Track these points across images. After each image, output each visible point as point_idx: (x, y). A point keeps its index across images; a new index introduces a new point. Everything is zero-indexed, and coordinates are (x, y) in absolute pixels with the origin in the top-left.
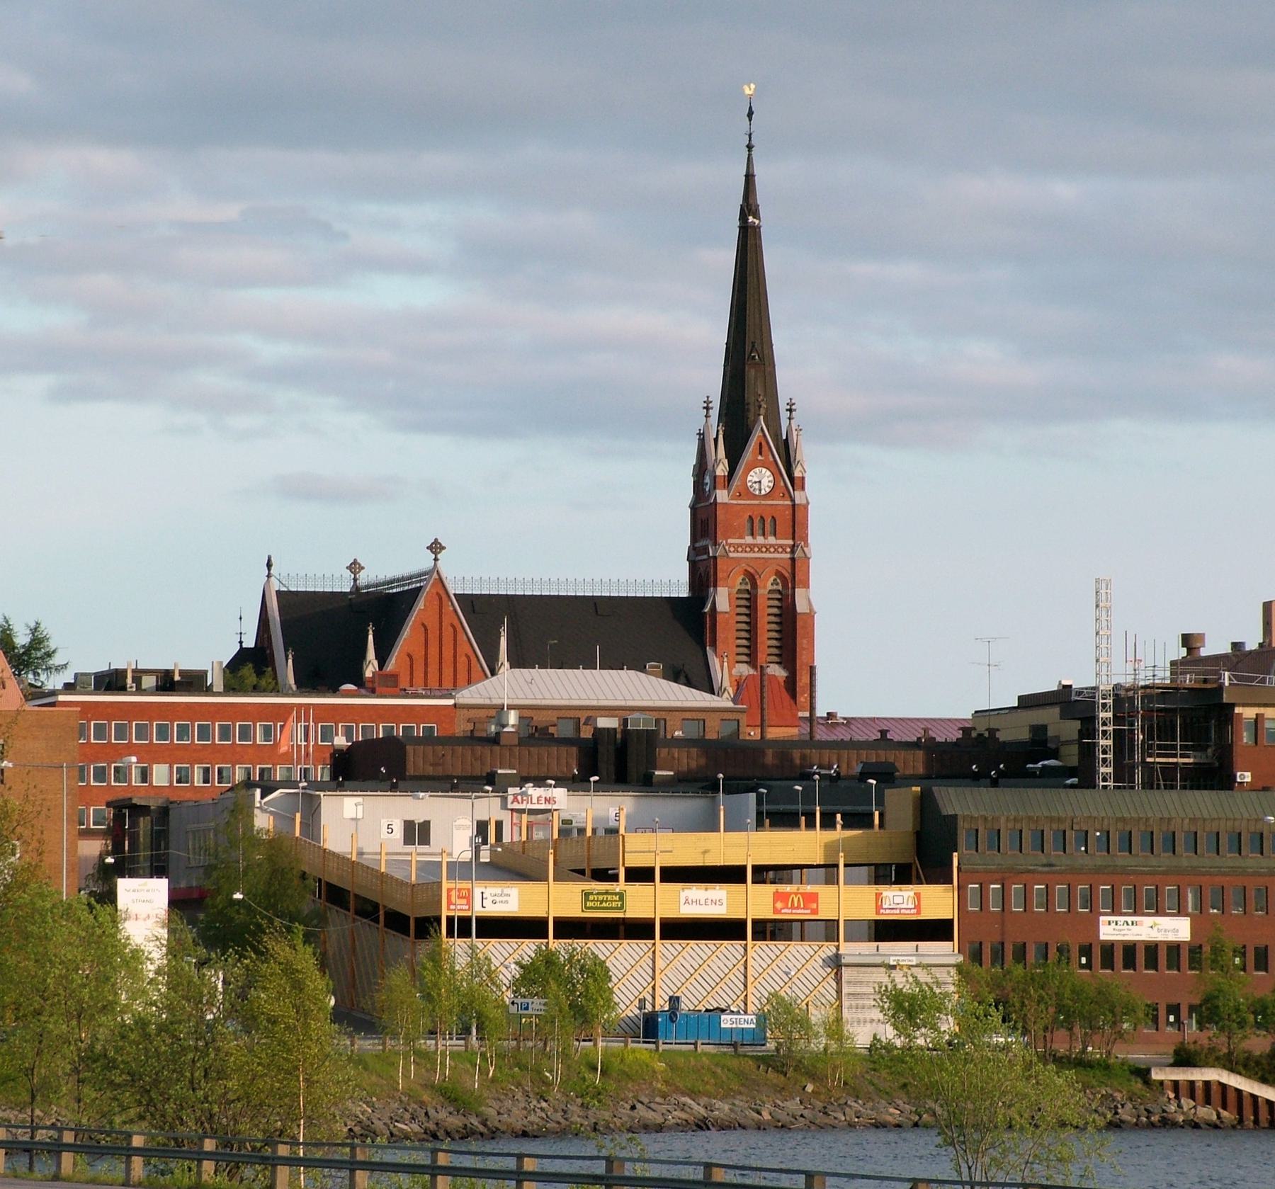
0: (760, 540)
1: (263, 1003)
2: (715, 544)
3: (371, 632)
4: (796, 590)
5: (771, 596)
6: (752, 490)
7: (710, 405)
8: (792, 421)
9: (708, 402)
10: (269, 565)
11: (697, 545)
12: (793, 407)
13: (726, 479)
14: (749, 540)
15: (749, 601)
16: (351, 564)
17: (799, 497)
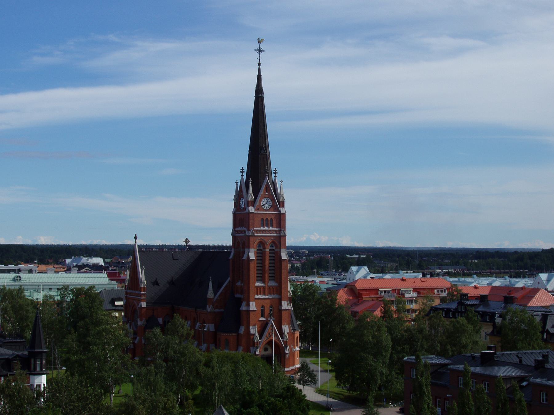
0: (266, 228)
1: (283, 370)
2: (249, 230)
3: (211, 279)
4: (282, 249)
5: (270, 252)
7: (243, 171)
9: (242, 169)
10: (136, 238)
11: (237, 229)
12: (276, 172)
13: (253, 202)
14: (262, 228)
15: (260, 254)
17: (282, 210)
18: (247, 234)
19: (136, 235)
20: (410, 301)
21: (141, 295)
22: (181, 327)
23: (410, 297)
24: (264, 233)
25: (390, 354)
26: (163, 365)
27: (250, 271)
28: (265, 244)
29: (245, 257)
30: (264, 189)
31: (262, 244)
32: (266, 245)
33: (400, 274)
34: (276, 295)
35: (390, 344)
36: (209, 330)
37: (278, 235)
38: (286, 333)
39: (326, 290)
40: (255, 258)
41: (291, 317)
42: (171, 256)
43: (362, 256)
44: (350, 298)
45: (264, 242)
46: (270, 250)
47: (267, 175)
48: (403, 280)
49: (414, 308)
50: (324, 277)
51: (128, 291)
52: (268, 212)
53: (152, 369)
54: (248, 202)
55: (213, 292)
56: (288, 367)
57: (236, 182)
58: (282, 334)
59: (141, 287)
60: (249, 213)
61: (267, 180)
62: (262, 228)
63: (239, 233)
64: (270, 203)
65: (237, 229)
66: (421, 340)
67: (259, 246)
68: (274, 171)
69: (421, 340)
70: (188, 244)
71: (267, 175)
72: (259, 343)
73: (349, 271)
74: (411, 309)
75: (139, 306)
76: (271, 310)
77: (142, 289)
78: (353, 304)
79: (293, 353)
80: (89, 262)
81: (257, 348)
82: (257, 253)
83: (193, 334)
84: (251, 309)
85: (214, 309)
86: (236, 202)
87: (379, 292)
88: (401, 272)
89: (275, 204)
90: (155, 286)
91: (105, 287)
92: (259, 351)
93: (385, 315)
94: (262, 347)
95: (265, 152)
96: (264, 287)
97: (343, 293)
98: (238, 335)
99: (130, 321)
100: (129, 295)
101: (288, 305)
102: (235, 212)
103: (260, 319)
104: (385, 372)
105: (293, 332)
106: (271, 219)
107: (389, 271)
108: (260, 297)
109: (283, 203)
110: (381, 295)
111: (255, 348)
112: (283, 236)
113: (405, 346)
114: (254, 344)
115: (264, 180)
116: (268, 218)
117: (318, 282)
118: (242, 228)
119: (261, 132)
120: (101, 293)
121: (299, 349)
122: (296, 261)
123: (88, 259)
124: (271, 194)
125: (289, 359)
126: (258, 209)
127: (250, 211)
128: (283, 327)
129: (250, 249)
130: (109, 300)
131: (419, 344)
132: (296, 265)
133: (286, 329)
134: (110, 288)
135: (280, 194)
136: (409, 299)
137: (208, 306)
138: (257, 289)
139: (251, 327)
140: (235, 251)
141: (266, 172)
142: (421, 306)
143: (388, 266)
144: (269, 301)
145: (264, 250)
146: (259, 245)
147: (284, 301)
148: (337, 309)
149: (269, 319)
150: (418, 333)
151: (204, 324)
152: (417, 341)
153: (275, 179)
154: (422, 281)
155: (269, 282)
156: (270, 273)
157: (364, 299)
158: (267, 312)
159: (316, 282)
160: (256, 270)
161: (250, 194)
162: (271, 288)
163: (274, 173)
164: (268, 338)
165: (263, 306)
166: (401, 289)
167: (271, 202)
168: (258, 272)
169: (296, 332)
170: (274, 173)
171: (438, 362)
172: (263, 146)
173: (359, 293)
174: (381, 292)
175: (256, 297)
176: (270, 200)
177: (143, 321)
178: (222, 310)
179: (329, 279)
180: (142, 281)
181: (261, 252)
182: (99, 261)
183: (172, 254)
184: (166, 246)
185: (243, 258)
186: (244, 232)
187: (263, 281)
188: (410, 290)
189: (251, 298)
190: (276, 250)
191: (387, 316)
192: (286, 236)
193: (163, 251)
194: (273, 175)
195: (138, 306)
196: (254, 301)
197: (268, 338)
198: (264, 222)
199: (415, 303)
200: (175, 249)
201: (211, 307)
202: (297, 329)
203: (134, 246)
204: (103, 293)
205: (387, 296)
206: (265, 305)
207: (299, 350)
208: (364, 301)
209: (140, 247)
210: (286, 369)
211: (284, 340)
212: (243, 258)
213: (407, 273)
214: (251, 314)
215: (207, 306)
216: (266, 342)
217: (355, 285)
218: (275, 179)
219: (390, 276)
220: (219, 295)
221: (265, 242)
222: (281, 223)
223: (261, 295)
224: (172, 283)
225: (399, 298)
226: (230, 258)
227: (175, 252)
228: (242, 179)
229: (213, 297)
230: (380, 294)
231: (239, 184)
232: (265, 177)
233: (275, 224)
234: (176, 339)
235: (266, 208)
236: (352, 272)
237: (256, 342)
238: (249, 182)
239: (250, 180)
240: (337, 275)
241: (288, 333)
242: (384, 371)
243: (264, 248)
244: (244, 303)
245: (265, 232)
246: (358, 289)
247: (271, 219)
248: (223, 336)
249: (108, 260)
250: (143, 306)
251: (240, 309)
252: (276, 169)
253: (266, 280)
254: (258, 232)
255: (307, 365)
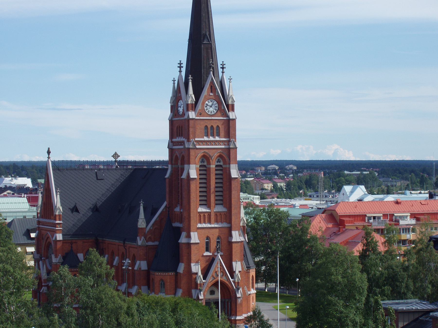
0: (211, 138)
2: (189, 141)
3: (142, 204)
5: (217, 168)
6: (207, 111)
7: (182, 65)
8: (224, 74)
9: (180, 64)
10: (49, 152)
11: (174, 140)
12: (224, 66)
13: (194, 105)
14: (206, 139)
16: (114, 155)
17: (232, 115)
18: (187, 147)
19: (49, 149)
20: (407, 230)
21: (55, 225)
22: (99, 265)
23: (407, 225)
24: (208, 145)
25: (366, 299)
26: (73, 313)
27: (191, 193)
28: (210, 159)
29: (184, 176)
30: (208, 88)
31: (206, 158)
32: (212, 159)
33: (406, 195)
34: (224, 223)
35: (366, 285)
36: (140, 268)
37: (227, 147)
38: (237, 272)
39: (301, 216)
40: (196, 177)
41: (245, 250)
42: (95, 176)
43: (365, 173)
44: (330, 226)
45: (208, 156)
46: (217, 166)
47: (212, 71)
48: (397, 203)
49: (411, 238)
50: (312, 199)
51: (41, 220)
52: (213, 118)
53: (55, 319)
54: (188, 105)
55: (145, 220)
56: (241, 315)
57: (172, 81)
58: (232, 273)
59: (56, 215)
60: (189, 120)
61: (212, 78)
62: (206, 139)
63: (177, 145)
64: (216, 107)
65: (174, 140)
66: (406, 279)
67: (202, 161)
68: (221, 65)
69: (406, 279)
70: (117, 160)
71: (212, 71)
72: (203, 284)
73: (342, 192)
74: (407, 240)
75: (54, 239)
76: (218, 242)
77: (57, 218)
78: (332, 234)
79: (247, 297)
80: (12, 183)
81: (201, 291)
82: (200, 170)
83: (113, 274)
84: (192, 242)
85: (147, 242)
86: (173, 105)
87: (366, 218)
88: (408, 192)
89: (222, 107)
90: (75, 213)
91: (24, 214)
92: (203, 295)
93: (367, 248)
94: (207, 289)
95: (209, 41)
96: (209, 214)
97: (321, 220)
98: (177, 274)
99: (43, 258)
100: (42, 225)
101: (239, 236)
102: (171, 119)
103: (204, 254)
104: (358, 321)
105: (247, 270)
106: (218, 126)
107: (397, 191)
108: (204, 225)
109: (233, 106)
110: (368, 222)
111: (198, 291)
112: (233, 148)
113: (386, 287)
114: (196, 286)
115: (207, 77)
116: (213, 125)
117: (297, 206)
118: (179, 138)
119: (204, 15)
120: (13, 223)
121: (256, 292)
122: (280, 179)
123: (12, 179)
124: (217, 94)
125: (241, 304)
126: (200, 114)
127: (191, 117)
128: (234, 263)
129: (191, 165)
130: (24, 232)
131: (404, 285)
132: (279, 184)
133: (238, 266)
134: (30, 216)
135: (229, 95)
136: (406, 227)
137: (138, 238)
138: (200, 216)
139: (192, 265)
140: (172, 167)
141: (210, 67)
142: (418, 236)
143: (397, 185)
144: (217, 230)
145: (208, 166)
146: (202, 160)
147: (235, 230)
148: (308, 241)
149: (216, 254)
150: (402, 270)
151: (123, 261)
152: (400, 280)
153: (223, 75)
154: (422, 204)
155: (216, 207)
156: (216, 196)
157: (346, 228)
158: (213, 245)
159: (295, 206)
160: (198, 192)
161: (189, 95)
162: (218, 214)
163: (221, 68)
164: (215, 278)
165: (208, 238)
166: (367, 215)
167: (217, 105)
168: (202, 194)
169: (251, 270)
170: (221, 68)
171: (419, 307)
172: (206, 34)
173: (340, 220)
174: (370, 218)
175: (199, 225)
176: (215, 102)
177: (59, 257)
178: (156, 243)
179: (318, 202)
180: (57, 207)
181: (204, 168)
182: (27, 182)
183: (96, 173)
184: (87, 162)
185: (182, 177)
186: (182, 143)
187: (209, 207)
188: (407, 216)
189: (192, 228)
190: (224, 166)
191: (371, 249)
192: (237, 148)
193: (84, 169)
194: (220, 70)
195: (52, 238)
196: (196, 231)
197: (215, 278)
198: (209, 130)
199: (413, 232)
200: (98, 166)
201: (142, 239)
202: (253, 266)
203: (47, 163)
204: (15, 222)
205: (377, 223)
206: (211, 236)
207: (256, 293)
208: (346, 229)
209: (54, 163)
210: (238, 318)
211: (235, 281)
212: (182, 177)
213: (420, 193)
214: (193, 247)
215: (138, 238)
216: (212, 283)
217: (336, 210)
218: (223, 75)
219: (394, 198)
220: (153, 224)
221: (210, 156)
222: (230, 132)
223: (205, 222)
224: (95, 209)
225: (390, 226)
226: (166, 177)
227: (100, 169)
228: (180, 75)
229: (145, 227)
230: (368, 220)
231: (176, 82)
232: (209, 73)
233: (222, 132)
234: (90, 280)
235: (211, 112)
236: (344, 194)
237: (198, 283)
238: (189, 79)
239: (189, 77)
240: (330, 196)
241: (239, 272)
242: (358, 319)
243: (209, 163)
244: (184, 234)
245: (209, 144)
246: (339, 214)
247: (218, 126)
248: (158, 276)
249: (167, 180)
250: (58, 239)
251: (179, 242)
252: (224, 63)
253: (213, 204)
254: (201, 144)
255: (259, 313)
